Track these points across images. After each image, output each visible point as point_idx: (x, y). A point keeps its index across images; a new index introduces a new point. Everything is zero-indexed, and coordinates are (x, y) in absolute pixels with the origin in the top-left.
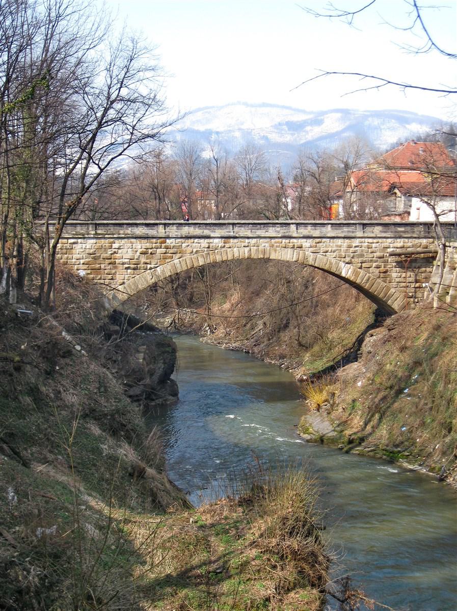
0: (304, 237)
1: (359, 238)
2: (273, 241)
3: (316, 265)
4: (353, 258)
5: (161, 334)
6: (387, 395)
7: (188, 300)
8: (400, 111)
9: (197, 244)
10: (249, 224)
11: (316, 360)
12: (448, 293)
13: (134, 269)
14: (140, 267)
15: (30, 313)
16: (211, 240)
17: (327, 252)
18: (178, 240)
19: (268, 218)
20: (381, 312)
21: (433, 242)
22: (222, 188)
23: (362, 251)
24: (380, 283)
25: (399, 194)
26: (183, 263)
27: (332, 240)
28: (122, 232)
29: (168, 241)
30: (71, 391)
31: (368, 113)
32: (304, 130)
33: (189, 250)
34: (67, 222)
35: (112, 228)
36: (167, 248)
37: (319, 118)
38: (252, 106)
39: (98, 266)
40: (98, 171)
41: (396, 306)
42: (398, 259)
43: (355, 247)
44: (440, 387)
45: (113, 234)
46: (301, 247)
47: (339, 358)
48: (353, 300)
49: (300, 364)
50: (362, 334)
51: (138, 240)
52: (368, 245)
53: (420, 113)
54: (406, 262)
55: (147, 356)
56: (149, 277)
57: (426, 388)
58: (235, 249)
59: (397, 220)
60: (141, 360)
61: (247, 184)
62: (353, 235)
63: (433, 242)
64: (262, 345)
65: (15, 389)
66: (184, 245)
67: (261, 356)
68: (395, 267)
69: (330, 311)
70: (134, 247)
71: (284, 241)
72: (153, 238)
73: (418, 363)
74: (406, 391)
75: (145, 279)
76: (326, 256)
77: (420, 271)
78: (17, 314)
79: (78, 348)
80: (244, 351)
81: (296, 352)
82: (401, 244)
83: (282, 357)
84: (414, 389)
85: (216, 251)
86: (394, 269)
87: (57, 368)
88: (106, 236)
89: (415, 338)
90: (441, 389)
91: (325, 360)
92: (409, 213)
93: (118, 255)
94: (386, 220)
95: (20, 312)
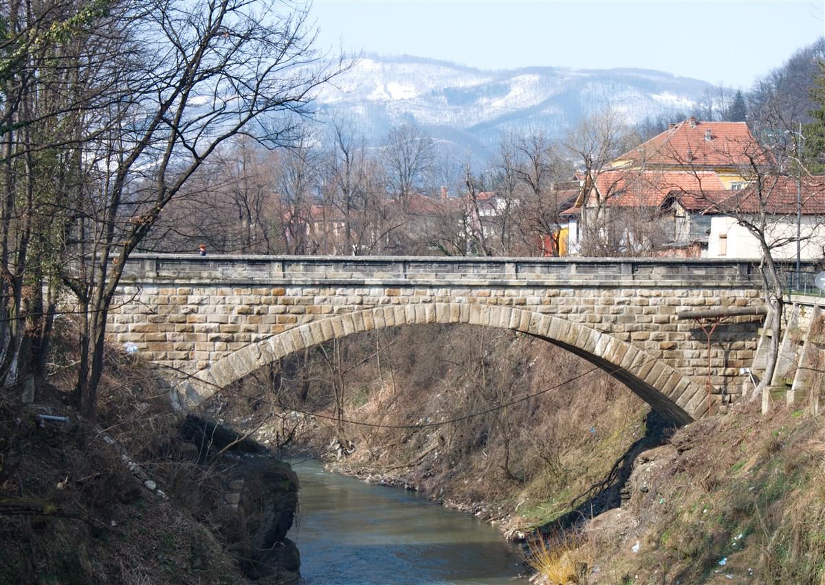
0: (529, 286)
1: (626, 287)
2: (475, 292)
3: (550, 335)
4: (615, 322)
5: (270, 458)
6: (687, 569)
7: (299, 396)
8: (635, 70)
9: (340, 298)
10: (432, 262)
11: (539, 504)
12: (790, 386)
13: (227, 341)
14: (238, 338)
15: (64, 422)
16: (366, 291)
17: (569, 312)
18: (306, 290)
19: (447, 254)
20: (662, 420)
21: (757, 296)
22: (358, 201)
23: (631, 310)
24: (663, 367)
25: (681, 212)
26: (316, 331)
27: (577, 292)
28: (205, 274)
29: (288, 291)
30: (140, 567)
31: (586, 75)
32: (476, 103)
33: (326, 307)
34: (131, 255)
35: (187, 267)
36: (286, 303)
37: (502, 83)
38: (385, 60)
39: (160, 335)
40: (190, 161)
41: (691, 409)
42: (694, 324)
43: (619, 303)
44: (790, 557)
45: (190, 278)
46: (524, 304)
47: (583, 499)
48: (603, 397)
49: (510, 511)
50: (625, 457)
51: (235, 290)
52: (641, 301)
53: (676, 74)
54: (709, 332)
55: (245, 497)
56: (254, 356)
57: (762, 558)
58: (408, 307)
59: (681, 256)
60: (236, 506)
61: (402, 194)
62: (615, 282)
63: (757, 296)
64: (438, 477)
65: (34, 567)
66: (317, 299)
67: (438, 496)
68: (690, 339)
69: (561, 416)
70: (227, 301)
71: (494, 292)
72: (262, 285)
73: (742, 511)
74: (723, 562)
75: (248, 359)
76: (567, 319)
77: (733, 347)
78: (38, 423)
79: (151, 485)
80: (406, 486)
81: (502, 489)
82: (701, 299)
83: (477, 497)
84: (740, 560)
85: (374, 310)
86: (687, 342)
87: (114, 523)
88: (177, 281)
89: (732, 467)
90: (792, 560)
91: (556, 504)
92: (704, 246)
93: (197, 316)
94: (670, 256)
95: (45, 419)
